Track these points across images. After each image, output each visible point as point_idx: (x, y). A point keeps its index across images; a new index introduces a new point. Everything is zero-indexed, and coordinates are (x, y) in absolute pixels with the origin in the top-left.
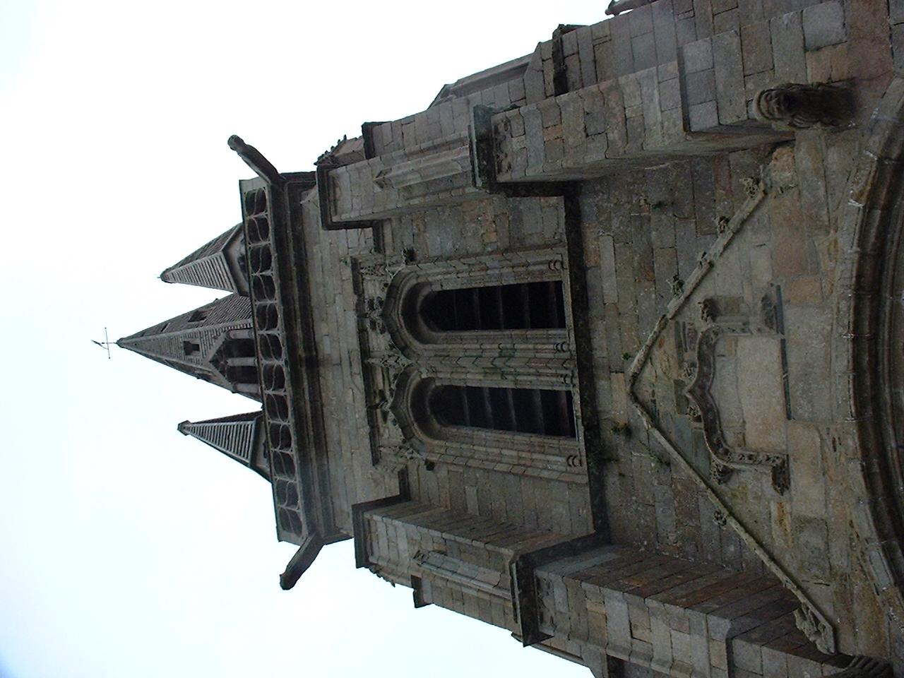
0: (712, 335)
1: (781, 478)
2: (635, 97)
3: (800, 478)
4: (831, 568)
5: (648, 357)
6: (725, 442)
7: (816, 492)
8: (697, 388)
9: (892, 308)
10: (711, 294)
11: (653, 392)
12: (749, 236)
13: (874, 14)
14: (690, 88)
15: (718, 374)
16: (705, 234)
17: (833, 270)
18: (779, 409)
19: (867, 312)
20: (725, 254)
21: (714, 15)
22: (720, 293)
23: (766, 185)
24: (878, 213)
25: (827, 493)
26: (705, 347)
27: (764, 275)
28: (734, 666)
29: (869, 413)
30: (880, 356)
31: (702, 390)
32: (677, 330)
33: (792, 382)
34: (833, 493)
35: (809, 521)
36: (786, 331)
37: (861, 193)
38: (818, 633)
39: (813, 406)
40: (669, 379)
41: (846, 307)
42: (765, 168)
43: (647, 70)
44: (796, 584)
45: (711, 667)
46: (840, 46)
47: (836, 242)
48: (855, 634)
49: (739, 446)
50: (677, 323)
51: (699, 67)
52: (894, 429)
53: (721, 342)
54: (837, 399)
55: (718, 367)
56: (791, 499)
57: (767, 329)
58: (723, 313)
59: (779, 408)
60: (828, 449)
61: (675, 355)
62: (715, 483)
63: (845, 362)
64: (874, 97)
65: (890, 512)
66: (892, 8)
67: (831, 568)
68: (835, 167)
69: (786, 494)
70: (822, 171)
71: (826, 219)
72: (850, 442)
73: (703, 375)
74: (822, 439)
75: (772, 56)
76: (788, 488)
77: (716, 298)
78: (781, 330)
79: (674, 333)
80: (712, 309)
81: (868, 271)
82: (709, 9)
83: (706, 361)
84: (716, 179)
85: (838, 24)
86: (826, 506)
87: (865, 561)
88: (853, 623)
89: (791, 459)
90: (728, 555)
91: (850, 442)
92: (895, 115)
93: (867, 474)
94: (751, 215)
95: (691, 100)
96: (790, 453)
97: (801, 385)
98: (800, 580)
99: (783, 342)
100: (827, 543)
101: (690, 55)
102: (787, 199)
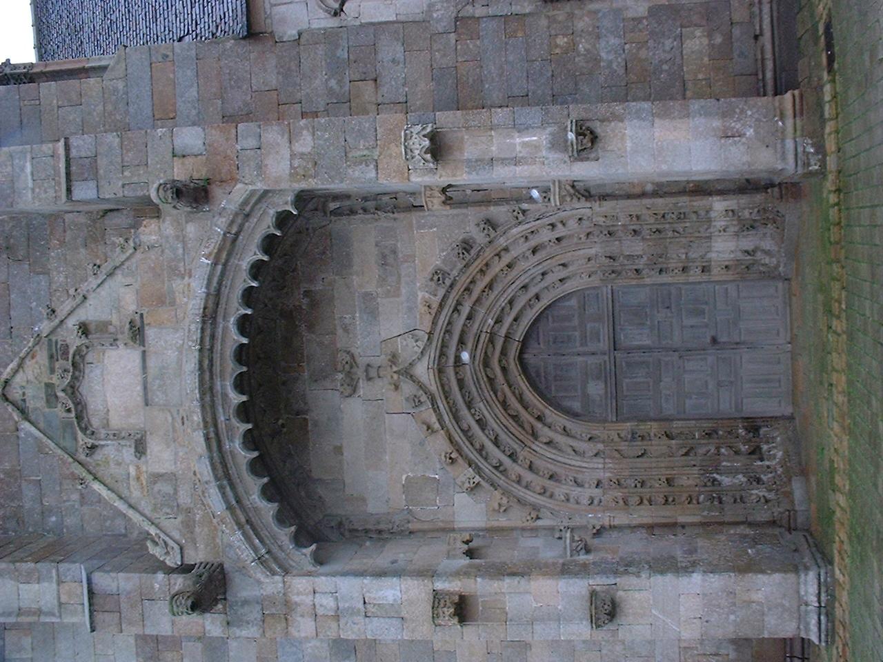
0: (84, 348)
1: (140, 448)
2: (6, 165)
3: (155, 447)
4: (178, 506)
5: (20, 366)
6: (91, 426)
7: (167, 455)
8: (68, 388)
9: (223, 330)
10: (83, 318)
11: (24, 394)
12: (119, 277)
13: (227, 140)
14: (73, 169)
15: (86, 377)
16: (38, 274)
17: (186, 304)
18: (140, 400)
19: (208, 332)
20: (98, 290)
21: (59, 107)
22: (90, 318)
23: (135, 243)
24: (219, 267)
25: (176, 454)
26: (77, 357)
27: (130, 304)
28: (93, 593)
29: (208, 398)
30: (214, 361)
31: (72, 390)
32: (50, 345)
33: (150, 380)
34: (181, 454)
35: (162, 475)
36: (146, 345)
37: (210, 254)
38: (167, 553)
39: (167, 396)
40: (40, 382)
41: (195, 328)
42: (135, 232)
43: (21, 147)
44: (150, 521)
45: (60, 604)
46: (200, 157)
47: (189, 285)
48: (196, 548)
49: (103, 428)
50: (50, 340)
51: (83, 154)
52: (223, 408)
53: (90, 354)
54: (186, 389)
55: (86, 371)
56: (147, 462)
57: (132, 343)
58: (93, 332)
59: (139, 399)
60: (178, 424)
61: (47, 364)
62: (82, 457)
63: (193, 365)
64: (224, 193)
65: (221, 463)
66: (239, 139)
67: (178, 506)
68: (191, 235)
69: (143, 459)
70: (181, 238)
71: (182, 269)
72: (196, 418)
73: (74, 378)
74: (173, 419)
75: (147, 156)
76: (144, 454)
77: (87, 322)
78: (143, 343)
79: (47, 348)
80: (84, 329)
81: (210, 305)
82: (55, 102)
83: (78, 365)
84: (51, 232)
85: (200, 142)
86: (175, 463)
87: (205, 497)
88: (194, 542)
89: (148, 433)
90: (50, 524)
91: (196, 418)
92: (237, 206)
93: (207, 439)
94: (122, 263)
95: (73, 177)
96: (146, 429)
97: (158, 381)
98: (153, 518)
99: (144, 352)
100: (175, 489)
101: (75, 144)
102: (152, 255)
